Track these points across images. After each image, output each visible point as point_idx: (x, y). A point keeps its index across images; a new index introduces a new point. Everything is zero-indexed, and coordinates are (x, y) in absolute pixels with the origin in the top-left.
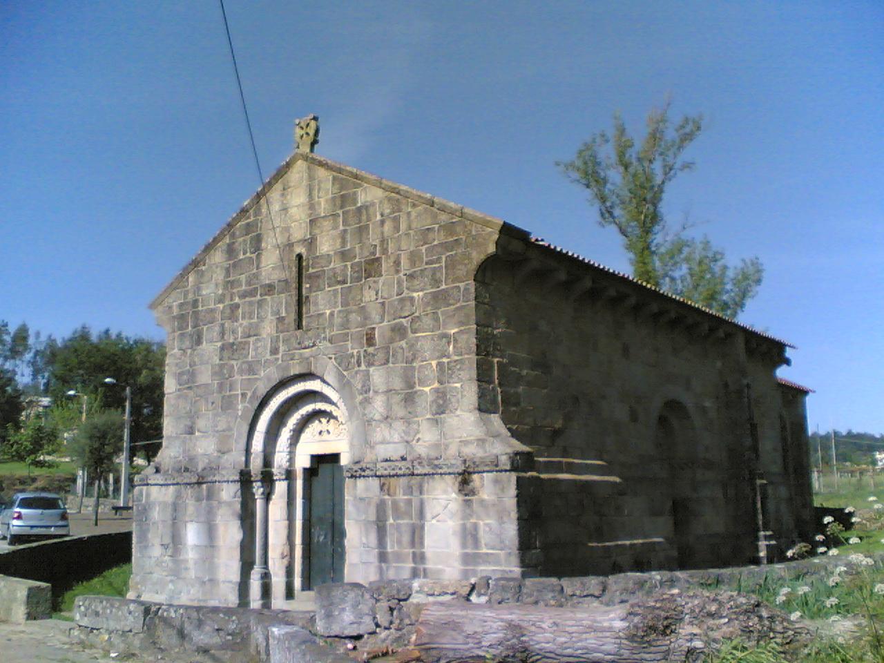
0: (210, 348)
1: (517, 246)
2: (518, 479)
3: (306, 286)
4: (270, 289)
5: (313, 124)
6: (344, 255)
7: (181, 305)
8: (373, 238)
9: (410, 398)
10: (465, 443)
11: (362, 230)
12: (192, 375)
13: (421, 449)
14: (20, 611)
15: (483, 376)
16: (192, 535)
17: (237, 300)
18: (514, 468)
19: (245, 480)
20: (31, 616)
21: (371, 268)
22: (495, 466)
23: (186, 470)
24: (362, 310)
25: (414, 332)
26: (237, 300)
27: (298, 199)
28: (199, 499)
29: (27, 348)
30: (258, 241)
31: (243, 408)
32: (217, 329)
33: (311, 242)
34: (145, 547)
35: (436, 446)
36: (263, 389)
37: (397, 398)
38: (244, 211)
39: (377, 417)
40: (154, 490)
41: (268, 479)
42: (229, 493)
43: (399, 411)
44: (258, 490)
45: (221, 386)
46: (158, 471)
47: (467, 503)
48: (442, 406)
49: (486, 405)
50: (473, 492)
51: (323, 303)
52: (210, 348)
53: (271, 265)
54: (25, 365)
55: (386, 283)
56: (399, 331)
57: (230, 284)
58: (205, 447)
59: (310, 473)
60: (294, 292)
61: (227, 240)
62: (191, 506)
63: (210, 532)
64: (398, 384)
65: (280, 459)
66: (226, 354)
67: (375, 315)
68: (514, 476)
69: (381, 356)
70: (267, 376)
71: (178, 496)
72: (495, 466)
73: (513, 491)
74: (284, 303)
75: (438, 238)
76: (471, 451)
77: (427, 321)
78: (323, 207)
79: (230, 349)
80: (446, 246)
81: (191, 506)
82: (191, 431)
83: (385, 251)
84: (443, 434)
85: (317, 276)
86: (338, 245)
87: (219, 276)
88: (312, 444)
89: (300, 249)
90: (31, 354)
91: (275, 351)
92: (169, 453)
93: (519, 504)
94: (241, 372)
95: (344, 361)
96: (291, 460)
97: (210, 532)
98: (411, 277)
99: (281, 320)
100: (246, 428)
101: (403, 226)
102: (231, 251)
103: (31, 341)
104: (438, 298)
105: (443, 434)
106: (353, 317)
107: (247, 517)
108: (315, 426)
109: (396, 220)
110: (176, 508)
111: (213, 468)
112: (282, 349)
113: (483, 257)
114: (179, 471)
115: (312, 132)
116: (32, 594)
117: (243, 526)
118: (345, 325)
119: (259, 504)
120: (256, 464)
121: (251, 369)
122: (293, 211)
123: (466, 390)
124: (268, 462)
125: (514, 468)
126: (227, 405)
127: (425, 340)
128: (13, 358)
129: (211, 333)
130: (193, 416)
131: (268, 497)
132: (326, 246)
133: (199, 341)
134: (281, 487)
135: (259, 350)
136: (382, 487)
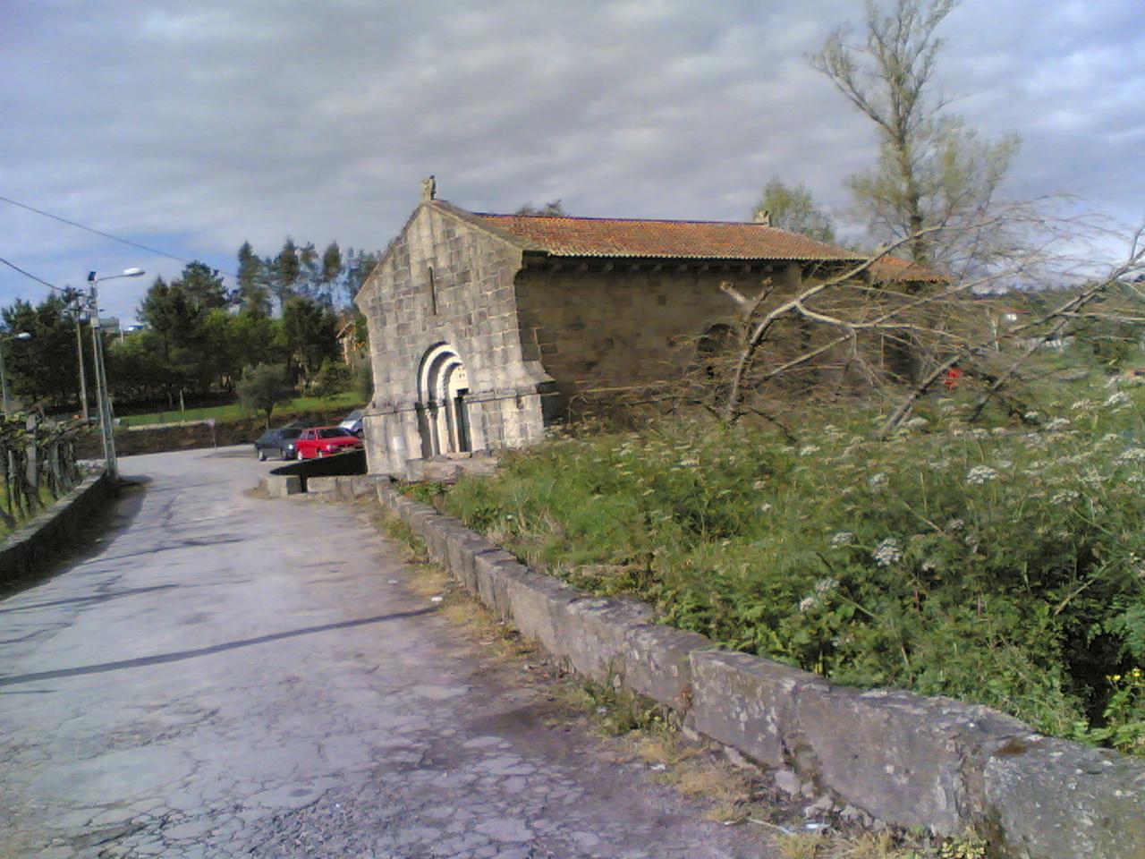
0: (391, 328)
1: (537, 260)
2: (542, 398)
3: (435, 288)
4: (417, 289)
5: (431, 181)
6: (452, 269)
7: (373, 300)
8: (465, 259)
9: (491, 355)
10: (518, 379)
11: (459, 253)
12: (384, 345)
13: (499, 385)
14: (284, 491)
15: (524, 339)
16: (396, 444)
17: (401, 297)
18: (539, 392)
19: (419, 408)
20: (289, 493)
21: (464, 277)
22: (529, 392)
23: (389, 405)
24: (464, 303)
25: (490, 315)
26: (401, 297)
27: (425, 232)
28: (396, 422)
29: (340, 269)
30: (407, 258)
31: (412, 364)
32: (394, 315)
33: (434, 260)
34: (372, 454)
35: (506, 382)
36: (421, 353)
37: (486, 355)
38: (398, 239)
39: (478, 367)
40: (373, 418)
41: (432, 406)
42: (411, 416)
43: (487, 363)
44: (428, 413)
45: (400, 351)
46: (374, 406)
47: (521, 413)
48: (506, 360)
49: (527, 357)
50: (522, 407)
51: (445, 299)
52: (391, 328)
53: (416, 276)
54: (340, 286)
55: (473, 285)
56: (482, 315)
57: (396, 287)
58: (396, 390)
59: (459, 400)
60: (430, 291)
61: (392, 258)
62: (393, 427)
63: (404, 441)
64: (485, 347)
65: (440, 394)
66: (400, 331)
67: (470, 306)
68: (539, 396)
69: (476, 331)
70: (422, 345)
71: (386, 421)
72: (529, 392)
73: (539, 405)
74: (422, 300)
75: (495, 259)
76: (521, 383)
77: (494, 310)
78: (439, 238)
79: (402, 328)
80: (499, 264)
81: (393, 427)
82: (388, 380)
83: (471, 266)
84: (508, 376)
85: (438, 282)
86: (448, 263)
87: (390, 281)
88: (458, 382)
89: (430, 265)
90: (347, 274)
91: (424, 329)
92: (378, 395)
93: (543, 411)
94: (409, 342)
95: (460, 335)
96: (446, 393)
97: (404, 441)
98: (485, 282)
99: (425, 309)
100: (416, 377)
101: (479, 251)
102: (394, 265)
103: (344, 261)
104: (498, 295)
105: (508, 376)
106: (460, 307)
107: (423, 429)
108: (456, 371)
109: (475, 248)
110: (385, 428)
111: (401, 403)
112: (428, 327)
113: (516, 271)
114: (385, 405)
115: (431, 187)
116: (289, 483)
117: (421, 436)
118: (457, 312)
119: (430, 422)
120: (425, 398)
121: (414, 341)
122: (423, 239)
123: (515, 349)
124: (432, 396)
125: (539, 392)
126: (404, 363)
127: (494, 319)
128: (326, 280)
129: (390, 317)
130: (387, 370)
131: (435, 417)
132: (442, 263)
133: (385, 325)
134: (441, 410)
135: (416, 328)
136: (483, 407)
